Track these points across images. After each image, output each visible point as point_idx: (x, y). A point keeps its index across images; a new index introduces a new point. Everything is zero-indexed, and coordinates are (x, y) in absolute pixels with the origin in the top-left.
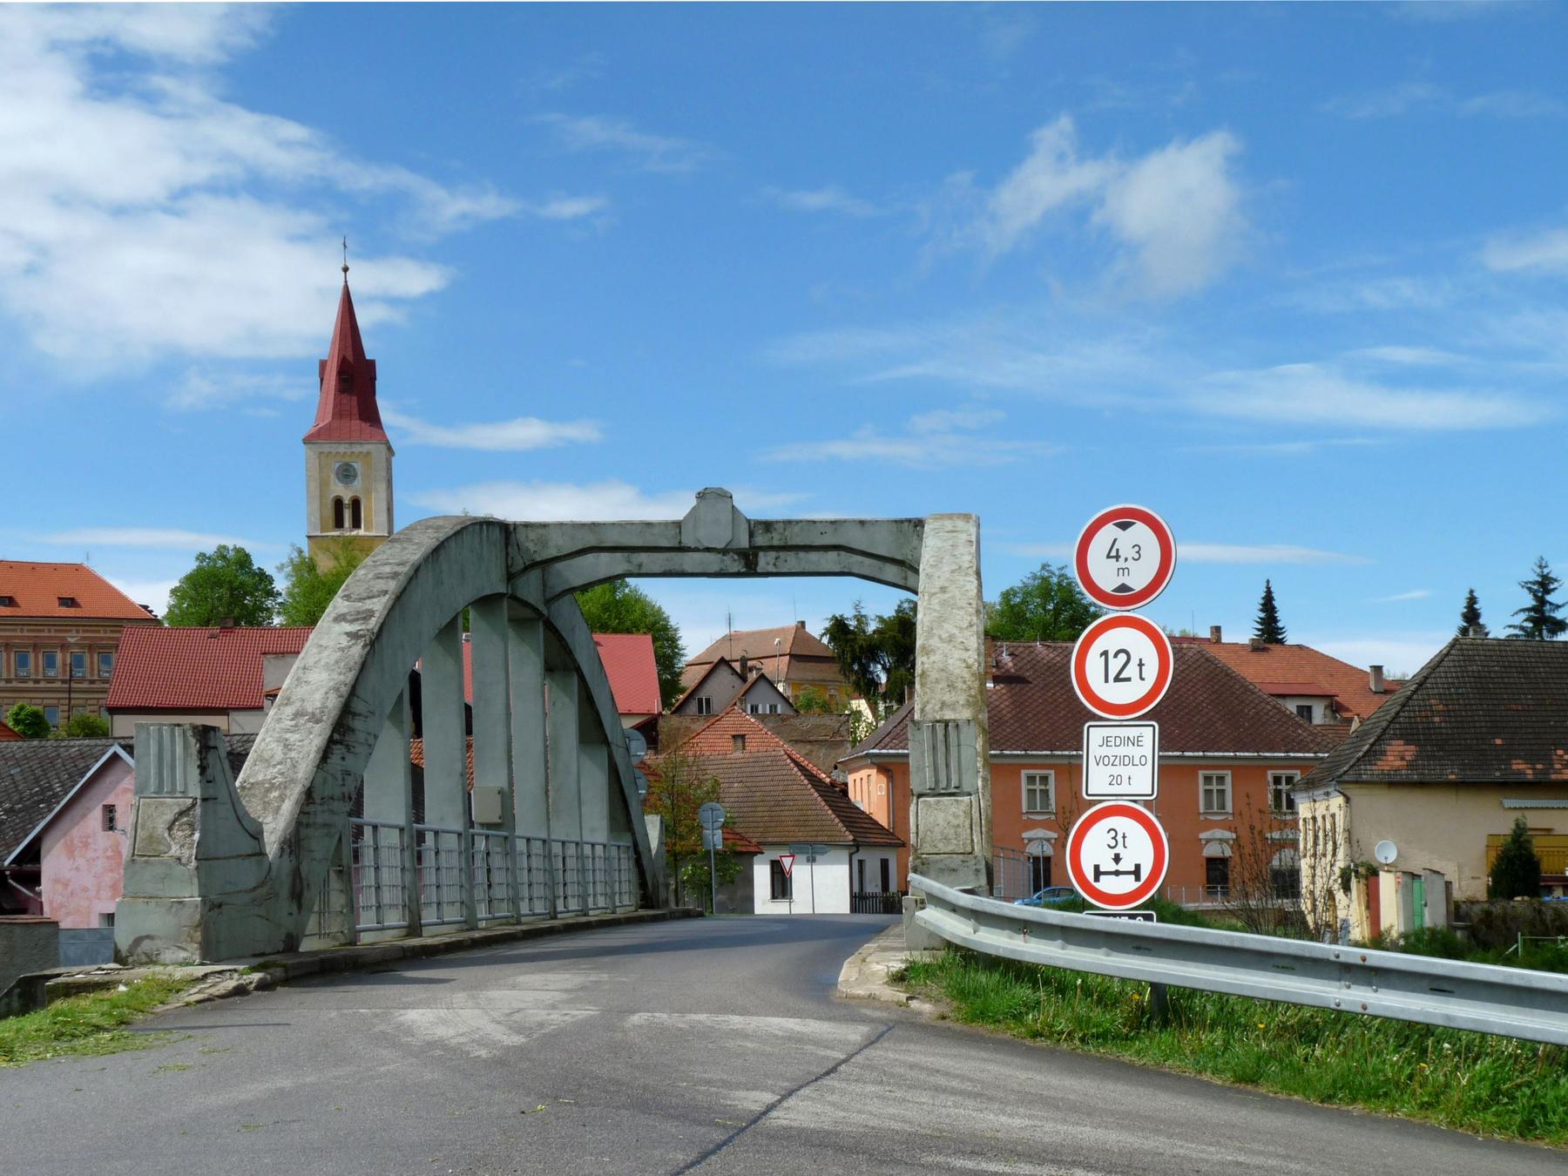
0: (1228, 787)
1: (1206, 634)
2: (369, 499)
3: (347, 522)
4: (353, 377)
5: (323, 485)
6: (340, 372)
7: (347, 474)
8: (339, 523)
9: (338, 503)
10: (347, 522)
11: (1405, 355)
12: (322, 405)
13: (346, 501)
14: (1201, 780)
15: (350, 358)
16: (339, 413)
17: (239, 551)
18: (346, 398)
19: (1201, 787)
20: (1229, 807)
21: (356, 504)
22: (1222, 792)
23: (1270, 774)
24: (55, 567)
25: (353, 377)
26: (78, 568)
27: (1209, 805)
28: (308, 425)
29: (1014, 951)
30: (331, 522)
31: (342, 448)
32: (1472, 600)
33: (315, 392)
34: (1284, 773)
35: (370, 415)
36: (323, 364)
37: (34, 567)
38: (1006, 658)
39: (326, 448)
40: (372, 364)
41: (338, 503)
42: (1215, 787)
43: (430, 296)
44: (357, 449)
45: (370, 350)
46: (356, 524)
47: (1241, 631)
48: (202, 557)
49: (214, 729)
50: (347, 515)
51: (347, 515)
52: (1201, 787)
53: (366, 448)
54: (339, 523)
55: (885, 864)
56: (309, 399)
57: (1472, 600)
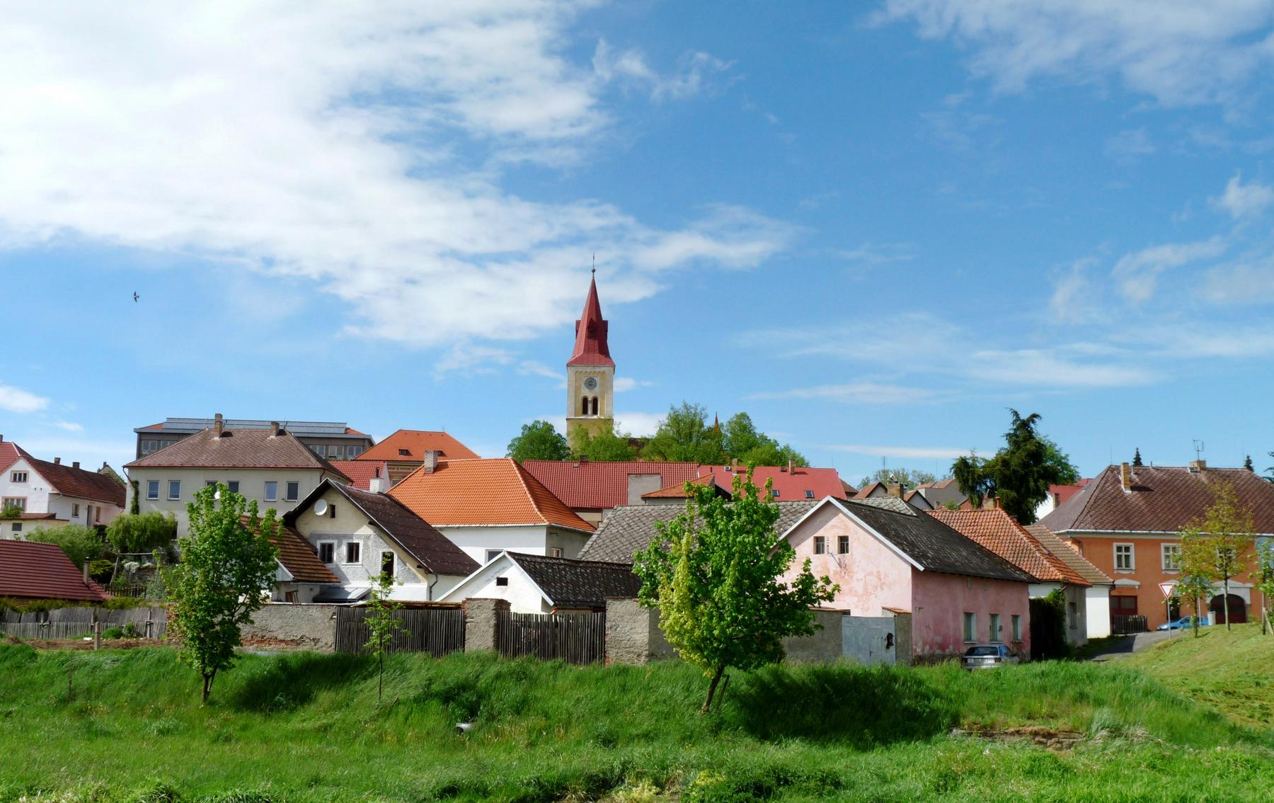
0: (1132, 553)
3: (590, 411)
4: (595, 330)
5: (577, 390)
6: (589, 328)
7: (591, 384)
8: (585, 412)
9: (585, 400)
10: (590, 411)
11: (1090, 348)
12: (577, 346)
16: (588, 349)
18: (591, 341)
19: (1115, 554)
20: (1133, 566)
21: (595, 401)
23: (1115, 545)
24: (430, 434)
25: (595, 330)
26: (443, 435)
27: (1120, 565)
28: (569, 357)
29: (69, 232)
30: (581, 411)
31: (589, 369)
32: (1138, 455)
33: (574, 340)
34: (1171, 545)
35: (604, 351)
36: (578, 323)
37: (418, 433)
39: (580, 369)
41: (585, 400)
42: (1123, 553)
43: (645, 302)
44: (597, 370)
45: (605, 315)
46: (595, 412)
49: (123, 506)
52: (1163, 553)
53: (603, 369)
54: (585, 412)
56: (571, 345)
57: (1138, 455)
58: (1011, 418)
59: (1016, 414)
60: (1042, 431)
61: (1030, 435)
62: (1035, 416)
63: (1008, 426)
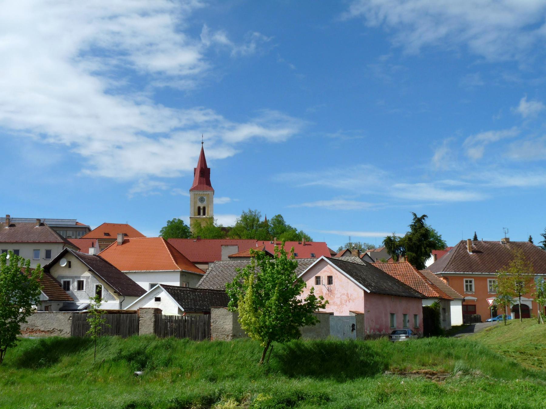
0: (473, 284)
1: (526, 240)
2: (208, 207)
4: (204, 173)
5: (195, 203)
7: (202, 200)
8: (199, 214)
9: (199, 208)
12: (195, 181)
13: (202, 208)
14: (465, 282)
15: (204, 167)
16: (200, 183)
17: (179, 220)
19: (465, 284)
21: (204, 208)
22: (471, 286)
24: (120, 225)
27: (467, 290)
28: (191, 186)
30: (197, 214)
31: (201, 193)
32: (476, 235)
35: (208, 183)
36: (195, 169)
38: (474, 246)
39: (196, 192)
40: (209, 169)
41: (199, 208)
42: (469, 284)
44: (205, 193)
45: (209, 165)
46: (204, 214)
47: (526, 240)
48: (169, 222)
50: (202, 211)
51: (202, 211)
54: (199, 214)
55: (200, 316)
56: (192, 180)
57: (476, 235)
58: (413, 217)
59: (415, 215)
60: (428, 223)
61: (422, 226)
62: (424, 216)
63: (411, 221)
